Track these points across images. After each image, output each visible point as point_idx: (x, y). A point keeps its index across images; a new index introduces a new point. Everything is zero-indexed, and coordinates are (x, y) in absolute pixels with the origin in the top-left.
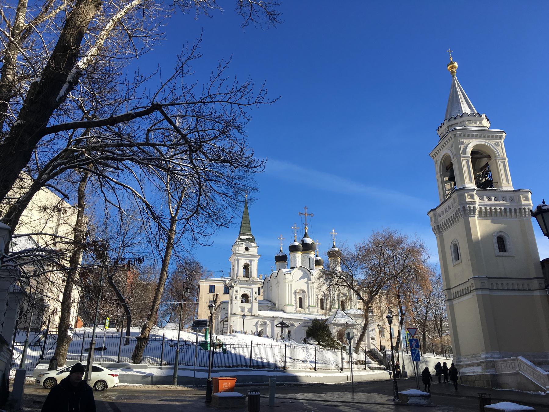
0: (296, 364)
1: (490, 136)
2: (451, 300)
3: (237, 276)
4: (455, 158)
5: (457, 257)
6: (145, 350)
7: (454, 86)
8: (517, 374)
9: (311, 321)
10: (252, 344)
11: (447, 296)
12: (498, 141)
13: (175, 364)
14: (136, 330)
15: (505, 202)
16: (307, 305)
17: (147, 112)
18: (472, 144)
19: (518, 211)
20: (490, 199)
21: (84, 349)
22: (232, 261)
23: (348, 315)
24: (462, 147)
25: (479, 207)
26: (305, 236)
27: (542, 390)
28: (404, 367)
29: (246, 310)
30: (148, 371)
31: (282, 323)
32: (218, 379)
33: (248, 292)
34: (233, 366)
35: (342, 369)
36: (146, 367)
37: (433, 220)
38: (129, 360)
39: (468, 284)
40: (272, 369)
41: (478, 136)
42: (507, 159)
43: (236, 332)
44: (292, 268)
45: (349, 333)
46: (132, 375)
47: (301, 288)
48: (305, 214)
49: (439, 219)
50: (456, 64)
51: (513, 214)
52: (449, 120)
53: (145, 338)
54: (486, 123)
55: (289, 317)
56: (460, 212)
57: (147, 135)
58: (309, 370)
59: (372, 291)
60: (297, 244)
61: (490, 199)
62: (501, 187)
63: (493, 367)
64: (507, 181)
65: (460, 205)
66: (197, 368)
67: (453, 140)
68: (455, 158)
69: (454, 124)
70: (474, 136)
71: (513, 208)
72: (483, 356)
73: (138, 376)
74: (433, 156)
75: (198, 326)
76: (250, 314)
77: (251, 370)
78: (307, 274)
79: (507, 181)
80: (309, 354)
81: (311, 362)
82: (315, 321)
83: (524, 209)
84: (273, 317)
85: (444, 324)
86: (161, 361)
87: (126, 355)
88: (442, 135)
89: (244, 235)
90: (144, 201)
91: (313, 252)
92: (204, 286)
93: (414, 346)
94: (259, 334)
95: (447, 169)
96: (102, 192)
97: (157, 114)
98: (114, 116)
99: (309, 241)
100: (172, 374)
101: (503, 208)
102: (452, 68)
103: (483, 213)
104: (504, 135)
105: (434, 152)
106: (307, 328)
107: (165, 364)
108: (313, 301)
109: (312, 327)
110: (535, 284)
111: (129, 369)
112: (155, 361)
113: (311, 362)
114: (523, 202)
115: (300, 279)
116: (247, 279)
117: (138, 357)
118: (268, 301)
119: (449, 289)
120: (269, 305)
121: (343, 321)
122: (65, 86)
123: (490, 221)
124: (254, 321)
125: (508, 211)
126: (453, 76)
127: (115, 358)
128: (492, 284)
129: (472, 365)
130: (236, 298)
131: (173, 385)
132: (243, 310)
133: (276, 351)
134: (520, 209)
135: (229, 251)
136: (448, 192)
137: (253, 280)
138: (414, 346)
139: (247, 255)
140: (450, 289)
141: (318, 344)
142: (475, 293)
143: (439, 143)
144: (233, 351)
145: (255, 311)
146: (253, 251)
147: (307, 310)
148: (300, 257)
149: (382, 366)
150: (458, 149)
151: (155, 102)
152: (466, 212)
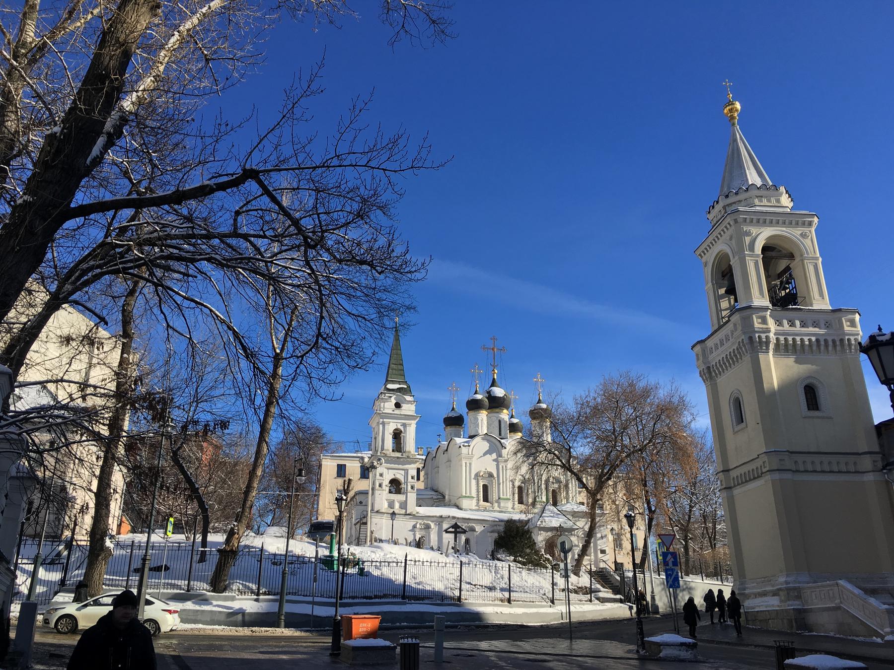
0: (478, 592)
1: (794, 223)
2: (730, 488)
3: (383, 449)
4: (737, 258)
5: (740, 418)
6: (232, 570)
7: (735, 140)
8: (838, 608)
9: (503, 523)
10: (406, 560)
11: (724, 483)
12: (806, 230)
13: (281, 594)
14: (217, 538)
15: (817, 329)
16: (495, 497)
17: (236, 183)
18: (763, 235)
19: (838, 343)
20: (792, 325)
21: (132, 569)
22: (374, 425)
23: (563, 513)
24: (748, 240)
25: (775, 337)
26: (493, 384)
27: (878, 635)
28: (653, 598)
29: (397, 505)
30: (236, 605)
31: (456, 526)
32: (351, 618)
33: (400, 476)
34: (376, 597)
35: (552, 602)
36: (233, 599)
37: (701, 358)
38: (206, 586)
39: (758, 463)
40: (438, 602)
41: (774, 221)
42: (820, 259)
43: (381, 541)
44: (472, 437)
45: (564, 542)
46: (211, 612)
47: (486, 470)
48: (493, 349)
49: (711, 357)
50: (738, 106)
51: (830, 348)
52: (727, 196)
53: (232, 551)
54: (785, 201)
55: (467, 516)
56: (744, 346)
57: (235, 220)
58: (500, 603)
59: (601, 473)
60: (479, 397)
61: (792, 325)
62: (811, 305)
63: (799, 597)
64: (821, 294)
65: (744, 333)
66: (317, 599)
67: (733, 227)
68: (737, 258)
69: (734, 203)
70: (767, 221)
71: (830, 339)
72: (782, 579)
73: (220, 612)
74: (700, 255)
75: (319, 531)
76: (403, 511)
77: (405, 604)
78: (496, 447)
79: (821, 294)
80: (499, 576)
81: (502, 590)
82: (510, 523)
83: (849, 340)
84: (441, 517)
85: (718, 527)
86: (259, 589)
87: (201, 579)
88: (715, 220)
89: (393, 382)
90: (229, 328)
91: (505, 411)
92: (329, 466)
93: (671, 564)
94: (419, 545)
95: (724, 276)
96: (162, 312)
97: (251, 186)
98: (181, 189)
99: (499, 392)
100: (277, 610)
101: (814, 339)
102: (731, 110)
103: (782, 347)
104: (816, 220)
105: (702, 248)
106: (496, 535)
107: (265, 594)
108: (505, 490)
109: (505, 532)
110: (867, 463)
111: (205, 600)
112: (249, 588)
113: (502, 590)
114: (846, 328)
115: (485, 454)
116: (398, 455)
117: (220, 582)
118: (433, 490)
119: (726, 471)
120: (435, 497)
121: (555, 523)
122: (101, 141)
123: (793, 360)
124: (410, 523)
125: (822, 343)
126: (734, 124)
127: (183, 583)
128: (796, 462)
129: (764, 594)
130: (380, 485)
131: (278, 627)
132: (391, 505)
133: (443, 572)
134: (842, 340)
135: (369, 410)
136: (724, 313)
137: (408, 457)
138: (671, 564)
139: (399, 416)
140: (728, 471)
141: (515, 561)
142: (768, 477)
143: (710, 233)
144: (376, 573)
145: (412, 507)
146: (409, 409)
147: (496, 505)
148: (485, 418)
149: (618, 597)
150: (740, 243)
151: (248, 167)
152: (754, 345)
